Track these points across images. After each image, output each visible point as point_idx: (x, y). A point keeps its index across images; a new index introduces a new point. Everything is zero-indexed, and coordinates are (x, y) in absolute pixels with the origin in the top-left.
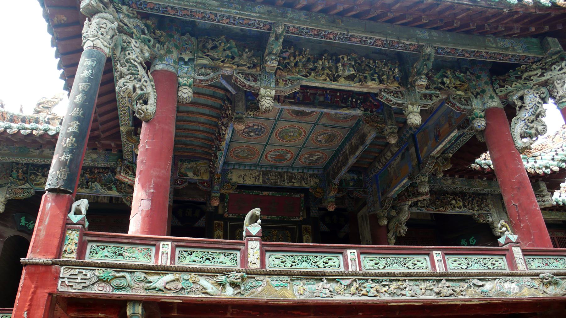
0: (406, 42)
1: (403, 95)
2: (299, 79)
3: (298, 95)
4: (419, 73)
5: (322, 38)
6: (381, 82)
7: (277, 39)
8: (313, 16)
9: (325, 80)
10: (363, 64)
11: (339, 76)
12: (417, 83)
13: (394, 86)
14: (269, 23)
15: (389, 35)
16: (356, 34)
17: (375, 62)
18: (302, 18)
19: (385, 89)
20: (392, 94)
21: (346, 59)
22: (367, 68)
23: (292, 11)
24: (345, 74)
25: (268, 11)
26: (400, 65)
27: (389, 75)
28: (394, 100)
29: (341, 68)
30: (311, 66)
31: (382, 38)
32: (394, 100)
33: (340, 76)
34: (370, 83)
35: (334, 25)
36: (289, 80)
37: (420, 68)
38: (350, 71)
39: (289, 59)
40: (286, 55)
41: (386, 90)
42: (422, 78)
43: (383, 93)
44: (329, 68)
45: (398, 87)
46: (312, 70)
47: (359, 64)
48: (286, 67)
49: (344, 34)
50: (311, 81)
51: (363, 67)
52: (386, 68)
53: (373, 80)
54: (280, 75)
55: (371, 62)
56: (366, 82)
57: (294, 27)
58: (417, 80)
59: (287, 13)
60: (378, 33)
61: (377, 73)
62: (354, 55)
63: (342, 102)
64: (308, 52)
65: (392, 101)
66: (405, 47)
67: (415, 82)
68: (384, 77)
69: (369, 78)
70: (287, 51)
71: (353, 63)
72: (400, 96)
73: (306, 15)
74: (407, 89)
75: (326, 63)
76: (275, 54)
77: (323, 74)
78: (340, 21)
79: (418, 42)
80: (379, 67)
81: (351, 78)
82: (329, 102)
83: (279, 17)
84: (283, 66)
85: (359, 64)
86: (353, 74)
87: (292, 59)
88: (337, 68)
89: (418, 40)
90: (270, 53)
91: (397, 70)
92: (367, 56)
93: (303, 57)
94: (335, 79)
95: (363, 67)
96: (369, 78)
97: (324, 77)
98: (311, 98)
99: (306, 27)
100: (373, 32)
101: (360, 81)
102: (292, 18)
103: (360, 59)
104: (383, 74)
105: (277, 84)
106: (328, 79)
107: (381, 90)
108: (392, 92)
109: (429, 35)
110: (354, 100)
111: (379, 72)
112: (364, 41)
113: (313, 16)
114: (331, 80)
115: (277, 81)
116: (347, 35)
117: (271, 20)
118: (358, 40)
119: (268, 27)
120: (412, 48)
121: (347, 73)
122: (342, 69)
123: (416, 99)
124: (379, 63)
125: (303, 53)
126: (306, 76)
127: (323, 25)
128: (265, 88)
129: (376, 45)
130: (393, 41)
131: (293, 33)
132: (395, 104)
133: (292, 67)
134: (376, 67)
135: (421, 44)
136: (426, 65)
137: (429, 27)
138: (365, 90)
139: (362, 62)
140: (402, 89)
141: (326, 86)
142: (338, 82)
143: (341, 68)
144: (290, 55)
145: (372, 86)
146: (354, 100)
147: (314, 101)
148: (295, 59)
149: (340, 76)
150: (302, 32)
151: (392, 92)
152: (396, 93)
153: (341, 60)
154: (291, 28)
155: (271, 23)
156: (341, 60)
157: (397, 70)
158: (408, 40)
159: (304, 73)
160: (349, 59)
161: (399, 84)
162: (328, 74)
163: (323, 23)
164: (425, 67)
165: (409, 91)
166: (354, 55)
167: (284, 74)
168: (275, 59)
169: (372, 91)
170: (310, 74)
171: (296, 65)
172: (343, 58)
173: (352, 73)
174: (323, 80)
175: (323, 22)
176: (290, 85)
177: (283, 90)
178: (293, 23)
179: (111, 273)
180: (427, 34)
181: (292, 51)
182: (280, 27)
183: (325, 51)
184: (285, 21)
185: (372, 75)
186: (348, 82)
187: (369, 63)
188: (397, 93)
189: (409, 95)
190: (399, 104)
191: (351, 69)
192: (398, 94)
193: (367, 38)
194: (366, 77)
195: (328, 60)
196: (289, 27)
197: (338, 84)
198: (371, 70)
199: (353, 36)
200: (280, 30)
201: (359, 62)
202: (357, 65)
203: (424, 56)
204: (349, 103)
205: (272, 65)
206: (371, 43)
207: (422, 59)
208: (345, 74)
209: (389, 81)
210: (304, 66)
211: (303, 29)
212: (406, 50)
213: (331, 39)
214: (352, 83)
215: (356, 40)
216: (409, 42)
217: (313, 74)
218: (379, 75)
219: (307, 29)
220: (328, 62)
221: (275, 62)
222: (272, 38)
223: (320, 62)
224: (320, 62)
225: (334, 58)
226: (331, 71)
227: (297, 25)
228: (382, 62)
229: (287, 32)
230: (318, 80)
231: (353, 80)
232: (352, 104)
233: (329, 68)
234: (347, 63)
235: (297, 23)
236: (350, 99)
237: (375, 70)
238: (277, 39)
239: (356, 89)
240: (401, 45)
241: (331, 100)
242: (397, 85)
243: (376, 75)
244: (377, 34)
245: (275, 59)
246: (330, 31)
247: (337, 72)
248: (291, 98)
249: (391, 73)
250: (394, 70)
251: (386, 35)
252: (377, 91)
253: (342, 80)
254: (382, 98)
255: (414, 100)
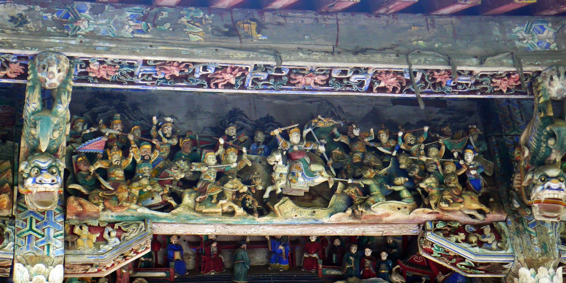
0: (478, 70)
1: (498, 235)
2: (144, 219)
3: (177, 255)
4: (540, 163)
5: (201, 86)
6: (420, 199)
7: (49, 99)
8: (164, 21)
9: (232, 214)
10: (358, 147)
11: (276, 197)
12: (533, 195)
13: (467, 209)
14: (19, 57)
15: (419, 52)
16: (308, 65)
17: (396, 138)
18: (127, 32)
19: (435, 222)
20: (462, 236)
21: (295, 138)
22: (370, 158)
23: (94, 11)
24: (295, 186)
25: (13, 19)
26: (484, 138)
27: (446, 175)
28: (472, 254)
29: (281, 169)
30: (177, 174)
31: (395, 67)
32: (472, 254)
33: (281, 196)
34: (382, 208)
35: (235, 42)
36: (112, 224)
37: (539, 147)
38: (312, 174)
39: (105, 157)
40: (95, 146)
41: (440, 226)
42: (548, 178)
43: (430, 236)
44: (244, 175)
45: (480, 211)
46: (189, 183)
47: (346, 149)
48: (98, 185)
49: (266, 68)
50: (186, 221)
51: (357, 157)
52: (433, 151)
53: (395, 196)
54: (78, 215)
55: (384, 137)
56: (368, 207)
57: (102, 62)
58: (534, 185)
59: (77, 19)
60: (382, 50)
61: (404, 173)
62: (324, 123)
63: (328, 263)
64: (168, 130)
65: (463, 259)
66: (477, 83)
67: (528, 190)
68: (429, 183)
69: (375, 189)
70: (99, 134)
71: (322, 149)
72: (490, 239)
73: (139, 20)
74: (514, 213)
75: (233, 157)
76: (52, 153)
77: (221, 196)
78: (254, 26)
79: (517, 63)
80: (409, 153)
81: (317, 197)
82: (285, 266)
83: (49, 35)
84: (82, 181)
85: (346, 149)
86: (326, 183)
87: (116, 156)
88: (270, 169)
89: (517, 57)
90: (34, 151)
91: (470, 156)
92: (364, 123)
93: (153, 147)
94: (265, 208)
95: (357, 157)
96: (375, 189)
97: (226, 204)
98: (225, 258)
99: (141, 58)
100: (364, 51)
101: (350, 203)
102: (92, 35)
103: (344, 132)
104: (425, 174)
105: (71, 240)
106: (240, 211)
107: (422, 226)
108: (461, 229)
109: (557, 38)
110: (368, 252)
111: (413, 169)
112: (341, 80)
113: (164, 21)
114: (250, 211)
115: (72, 233)
116: (279, 70)
117: (22, 46)
118: (319, 79)
119: (16, 68)
120: (503, 85)
121: (302, 184)
122: (285, 170)
123: (544, 246)
124: (410, 138)
125: (153, 132)
126: (166, 208)
127: (197, 46)
128: (29, 262)
129: (383, 90)
130: (432, 72)
131: (102, 80)
132: (476, 266)
133: (116, 185)
134: (400, 151)
135: (528, 69)
136: (552, 135)
137: (554, 12)
138: (372, 231)
139: (354, 140)
140: (494, 216)
141: (239, 231)
142: (275, 215)
143: (281, 169)
144: (108, 146)
145: (391, 218)
146: (368, 252)
147: (232, 270)
148: (126, 155)
149: (281, 196)
150: (132, 74)
151: (456, 231)
152: (473, 232)
153: (281, 141)
154: (94, 66)
155: (26, 58)
156: (281, 141)
157: (470, 156)
158: (481, 63)
159: (158, 199)
160: (310, 138)
161: (483, 200)
162: (238, 194)
163: (194, 38)
164: (551, 142)
165: (519, 220)
166: (324, 123)
167: (90, 208)
168: (49, 169)
169: (396, 231)
170: (179, 200)
171: (131, 174)
172: (286, 136)
173: (319, 180)
174: (225, 213)
175: (196, 35)
176: (114, 241)
177: (91, 260)
178: (94, 50)
179: (187, 222)
180: (548, 33)
181: (116, 130)
182: (54, 69)
183: (234, 116)
184: (68, 48)
185: (389, 179)
186: (306, 213)
187: (377, 140)
188: (479, 228)
189: (519, 232)
190: (489, 268)
191: (315, 168)
192: (482, 232)
193: (344, 72)
194: (366, 191)
195: (238, 145)
196: (87, 63)
197: (276, 221)
198: (386, 165)
199: (300, 71)
200: (54, 77)
201: (344, 140)
202: (337, 151)
203: (542, 109)
204: (351, 264)
205: (41, 188)
206: (361, 84)
207: (538, 117)
208: (295, 186)
209: (447, 196)
210: (159, 175)
211: (131, 65)
212: (483, 91)
213: (229, 85)
214: (322, 214)
215: (310, 81)
216: (488, 69)
217: (188, 200)
218: (411, 179)
219: (145, 63)
220: (240, 153)
221: (47, 178)
222: (33, 103)
223: (211, 158)
224: (211, 158)
225: (260, 137)
226: (247, 182)
227: (111, 57)
228: (417, 135)
229: (84, 76)
230: (205, 214)
231: (325, 204)
232: (362, 266)
233: (244, 175)
234: (301, 152)
235: (109, 50)
236: (354, 250)
237: (397, 163)
238: (49, 99)
239: (341, 231)
240: (463, 80)
241: (291, 258)
242: (477, 206)
243: (400, 180)
244: (379, 56)
245: (49, 169)
246: (220, 62)
247: (271, 182)
248: (157, 267)
249: (451, 168)
250: (462, 156)
251: (407, 54)
252: (411, 230)
253: (287, 207)
254: (431, 253)
255: (537, 249)
